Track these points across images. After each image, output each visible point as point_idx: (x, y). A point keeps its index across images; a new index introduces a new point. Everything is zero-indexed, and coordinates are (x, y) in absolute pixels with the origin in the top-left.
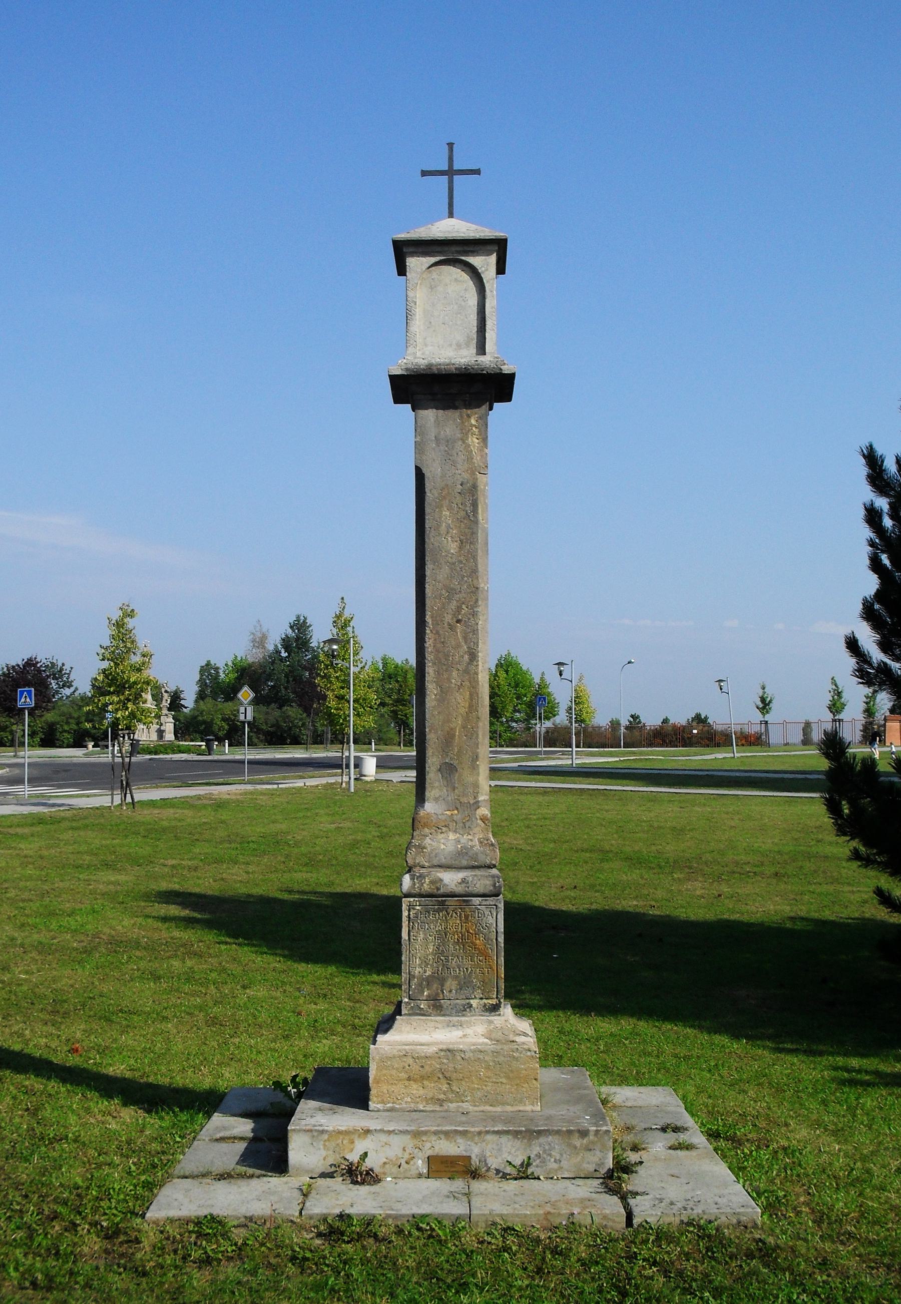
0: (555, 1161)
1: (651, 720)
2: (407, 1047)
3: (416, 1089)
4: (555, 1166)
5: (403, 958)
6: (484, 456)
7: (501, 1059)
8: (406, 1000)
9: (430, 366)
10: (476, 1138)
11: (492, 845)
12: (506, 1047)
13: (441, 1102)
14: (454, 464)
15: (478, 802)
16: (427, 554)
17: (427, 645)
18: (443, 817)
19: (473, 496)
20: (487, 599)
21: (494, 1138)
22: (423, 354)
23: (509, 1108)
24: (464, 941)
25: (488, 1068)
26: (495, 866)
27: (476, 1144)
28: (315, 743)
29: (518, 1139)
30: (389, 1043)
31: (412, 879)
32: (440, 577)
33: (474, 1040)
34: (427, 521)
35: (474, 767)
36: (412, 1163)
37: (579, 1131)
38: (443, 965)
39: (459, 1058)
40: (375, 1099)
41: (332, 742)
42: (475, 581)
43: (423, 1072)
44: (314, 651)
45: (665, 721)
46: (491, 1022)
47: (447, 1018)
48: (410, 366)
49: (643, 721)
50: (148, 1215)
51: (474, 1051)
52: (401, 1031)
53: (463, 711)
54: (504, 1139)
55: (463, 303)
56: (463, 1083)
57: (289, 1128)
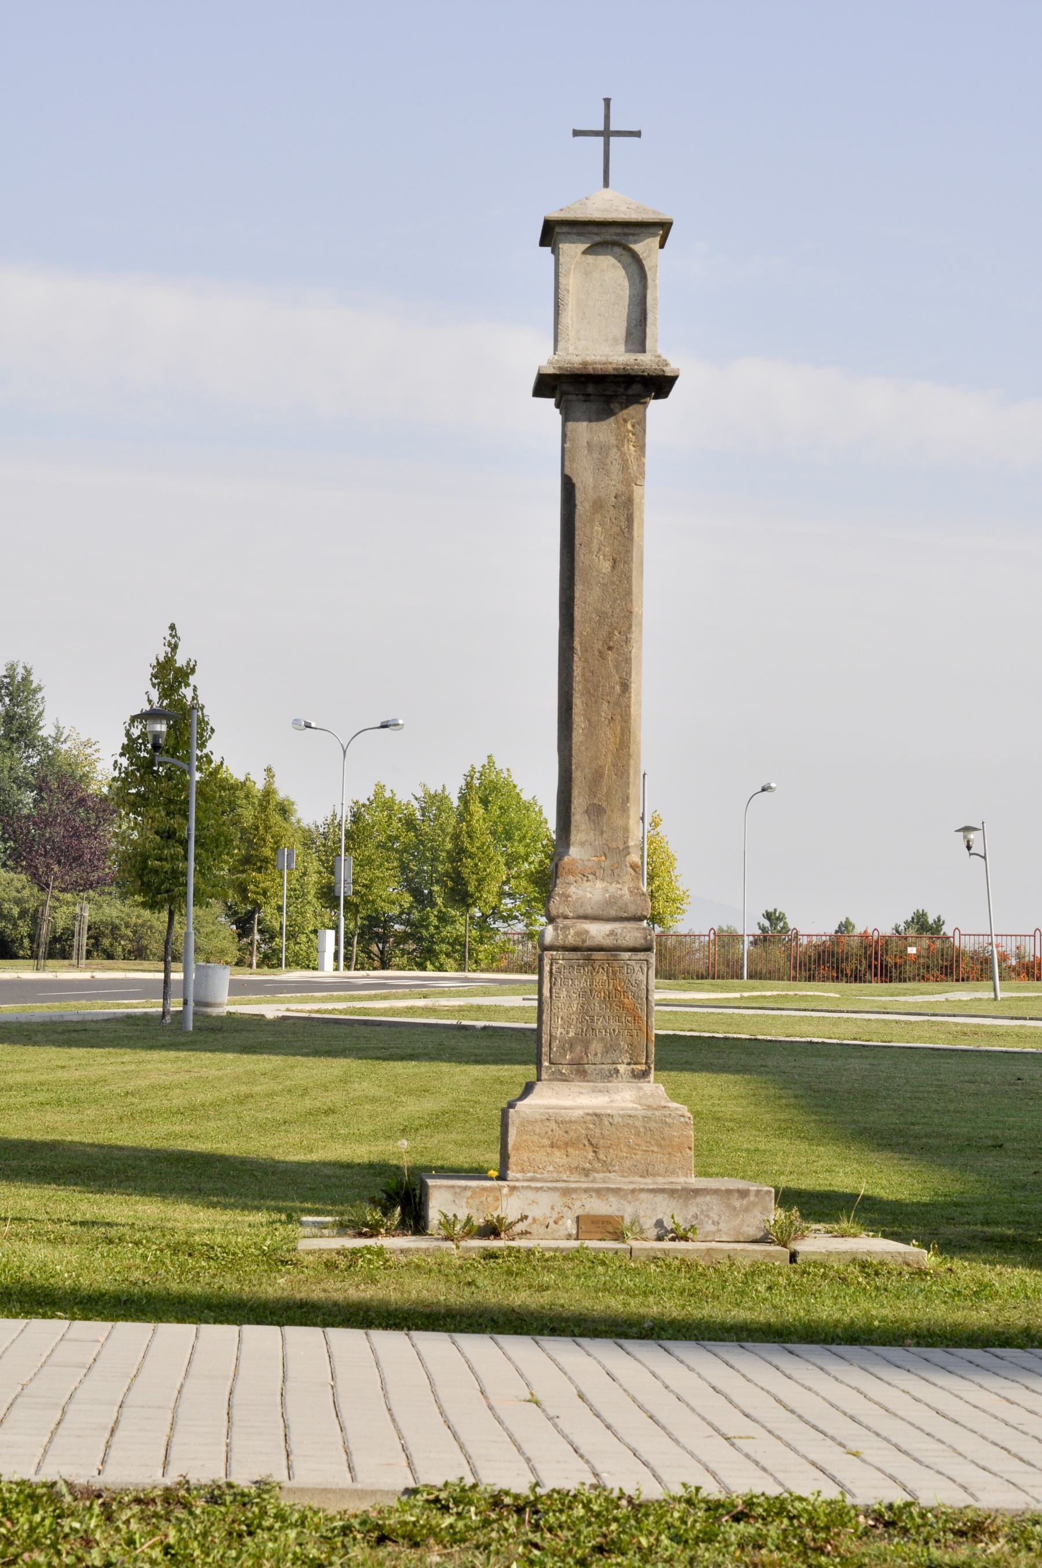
0: (713, 1223)
1: (813, 923)
3: (559, 1157)
4: (714, 1228)
6: (641, 466)
7: (652, 1125)
9: (585, 364)
10: (630, 1196)
11: (643, 894)
12: (657, 1113)
13: (586, 1172)
14: (608, 474)
16: (577, 573)
18: (590, 864)
19: (628, 510)
20: (641, 625)
21: (650, 1196)
22: (576, 349)
27: (629, 1202)
28: (51, 955)
30: (530, 1106)
31: (556, 929)
32: (590, 600)
33: (623, 1105)
34: (577, 537)
36: (560, 1223)
37: (738, 1191)
39: (607, 1123)
41: (89, 955)
42: (629, 605)
43: (567, 1138)
44: (48, 747)
45: (845, 927)
46: (641, 1088)
47: (591, 1084)
48: (562, 364)
51: (623, 1116)
53: (612, 747)
54: (660, 1198)
56: (611, 1151)
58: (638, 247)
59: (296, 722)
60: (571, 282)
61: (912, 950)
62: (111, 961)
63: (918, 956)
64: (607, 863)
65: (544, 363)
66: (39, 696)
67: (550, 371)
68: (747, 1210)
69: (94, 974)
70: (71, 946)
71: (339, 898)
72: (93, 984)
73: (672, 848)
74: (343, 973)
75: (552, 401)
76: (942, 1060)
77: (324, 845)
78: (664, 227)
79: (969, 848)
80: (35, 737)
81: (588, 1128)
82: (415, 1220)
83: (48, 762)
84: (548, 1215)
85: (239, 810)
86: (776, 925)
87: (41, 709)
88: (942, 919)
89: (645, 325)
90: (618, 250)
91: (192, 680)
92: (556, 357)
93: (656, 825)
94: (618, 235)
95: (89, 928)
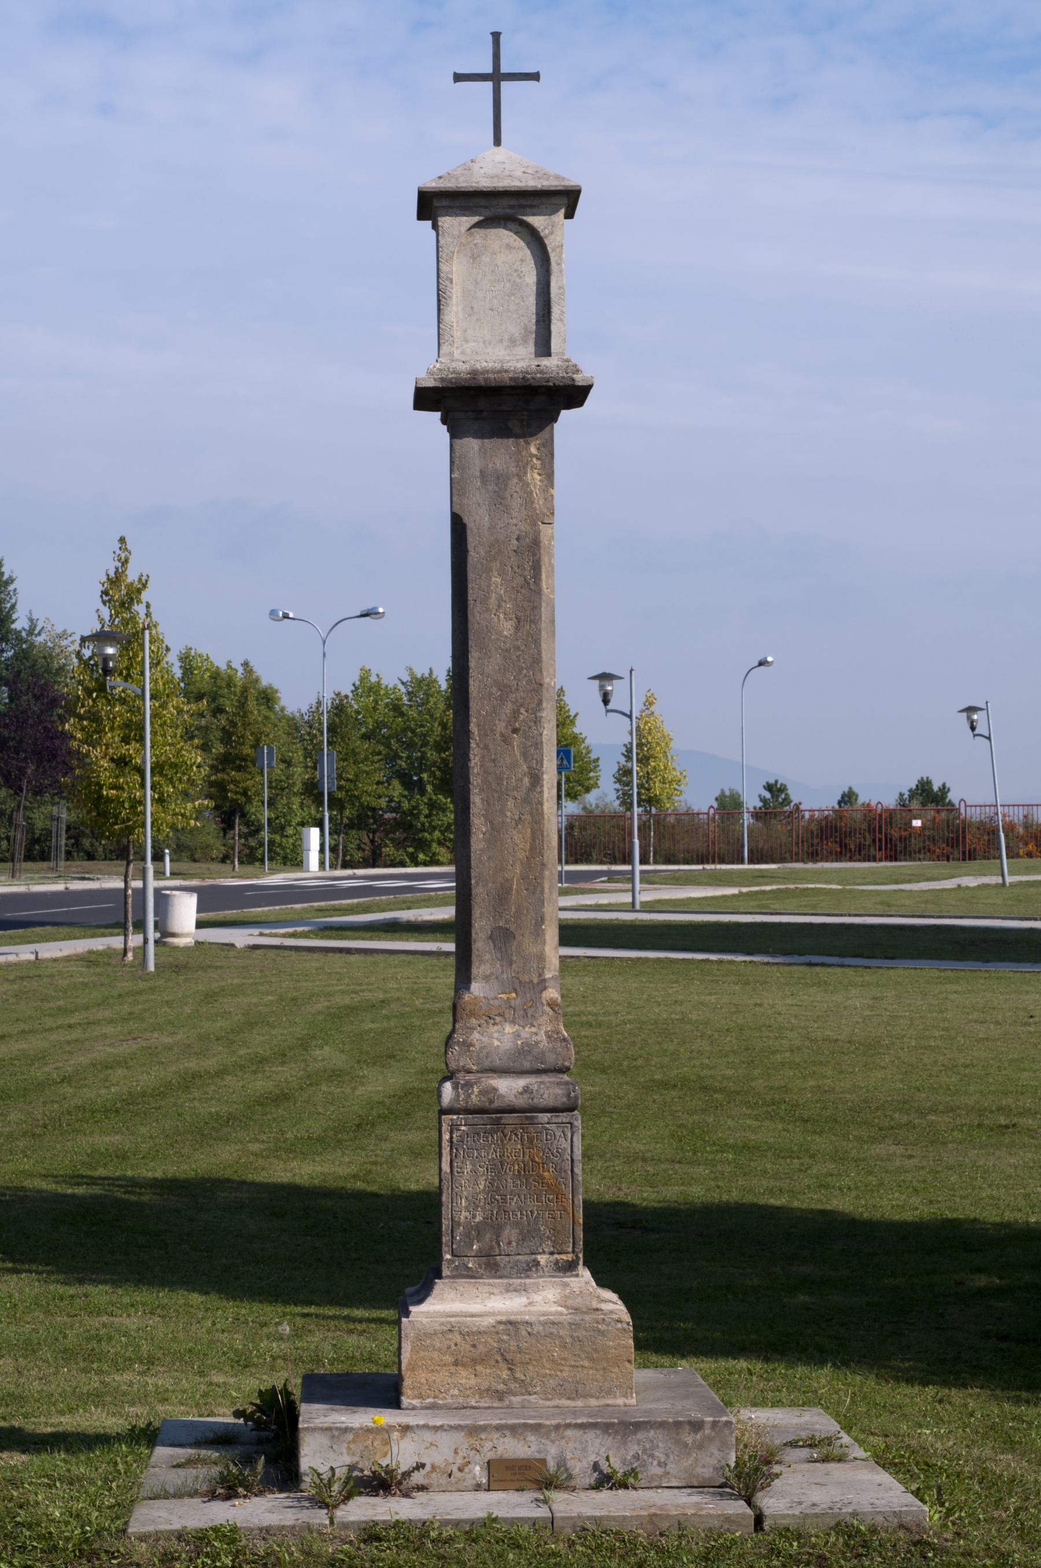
0: (659, 1464)
1: (815, 796)
2: (453, 1319)
3: (465, 1377)
4: (659, 1471)
5: (444, 1198)
6: (549, 499)
7: (581, 1333)
8: (448, 1257)
9: (474, 373)
10: (553, 1434)
11: (565, 1040)
12: (587, 1318)
13: (500, 1395)
14: (507, 509)
15: (544, 980)
16: (471, 636)
17: (472, 764)
18: (496, 1003)
19: (534, 555)
21: (578, 1433)
22: (462, 353)
23: (593, 1402)
24: (528, 1173)
25: (564, 1346)
26: (568, 1069)
27: (553, 1442)
28: (29, 857)
29: (609, 1434)
30: (427, 1314)
31: (455, 1087)
33: (545, 1308)
34: (470, 591)
35: (538, 933)
36: (466, 1470)
37: (690, 1423)
38: (499, 1207)
39: (524, 1333)
40: (409, 1392)
41: (69, 856)
42: (538, 675)
44: (20, 640)
45: (848, 798)
46: (566, 1285)
47: (506, 1281)
49: (795, 798)
50: (130, 1530)
51: (544, 1324)
52: (442, 1300)
53: (522, 855)
54: (590, 1435)
55: (518, 280)
56: (530, 1367)
57: (300, 1426)
58: (536, 221)
59: (273, 613)
60: (457, 268)
61: (917, 823)
62: (91, 862)
63: (924, 827)
64: (519, 1001)
65: (422, 374)
66: (11, 588)
67: (431, 383)
68: (700, 1447)
69: (68, 885)
70: (50, 847)
71: (322, 794)
72: (67, 897)
73: (667, 729)
74: (329, 873)
75: (438, 415)
76: (949, 987)
77: (309, 734)
78: (568, 199)
79: (973, 728)
80: (9, 631)
81: (501, 1341)
82: (285, 1474)
83: (23, 656)
84: (451, 1461)
85: (221, 700)
86: (778, 797)
87: (13, 601)
88: (947, 785)
89: (550, 320)
90: (511, 225)
91: (145, 596)
92: (438, 365)
93: (651, 704)
94: (512, 207)
95: (68, 828)
